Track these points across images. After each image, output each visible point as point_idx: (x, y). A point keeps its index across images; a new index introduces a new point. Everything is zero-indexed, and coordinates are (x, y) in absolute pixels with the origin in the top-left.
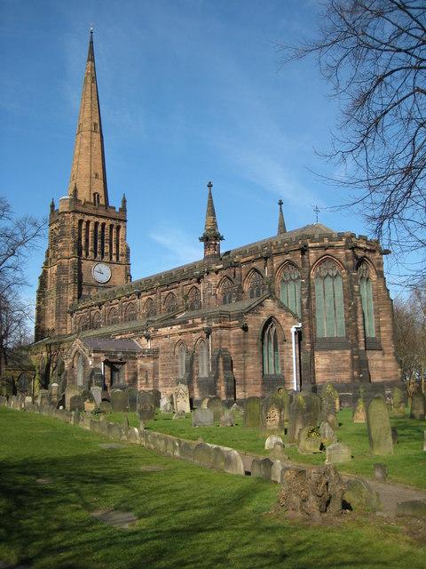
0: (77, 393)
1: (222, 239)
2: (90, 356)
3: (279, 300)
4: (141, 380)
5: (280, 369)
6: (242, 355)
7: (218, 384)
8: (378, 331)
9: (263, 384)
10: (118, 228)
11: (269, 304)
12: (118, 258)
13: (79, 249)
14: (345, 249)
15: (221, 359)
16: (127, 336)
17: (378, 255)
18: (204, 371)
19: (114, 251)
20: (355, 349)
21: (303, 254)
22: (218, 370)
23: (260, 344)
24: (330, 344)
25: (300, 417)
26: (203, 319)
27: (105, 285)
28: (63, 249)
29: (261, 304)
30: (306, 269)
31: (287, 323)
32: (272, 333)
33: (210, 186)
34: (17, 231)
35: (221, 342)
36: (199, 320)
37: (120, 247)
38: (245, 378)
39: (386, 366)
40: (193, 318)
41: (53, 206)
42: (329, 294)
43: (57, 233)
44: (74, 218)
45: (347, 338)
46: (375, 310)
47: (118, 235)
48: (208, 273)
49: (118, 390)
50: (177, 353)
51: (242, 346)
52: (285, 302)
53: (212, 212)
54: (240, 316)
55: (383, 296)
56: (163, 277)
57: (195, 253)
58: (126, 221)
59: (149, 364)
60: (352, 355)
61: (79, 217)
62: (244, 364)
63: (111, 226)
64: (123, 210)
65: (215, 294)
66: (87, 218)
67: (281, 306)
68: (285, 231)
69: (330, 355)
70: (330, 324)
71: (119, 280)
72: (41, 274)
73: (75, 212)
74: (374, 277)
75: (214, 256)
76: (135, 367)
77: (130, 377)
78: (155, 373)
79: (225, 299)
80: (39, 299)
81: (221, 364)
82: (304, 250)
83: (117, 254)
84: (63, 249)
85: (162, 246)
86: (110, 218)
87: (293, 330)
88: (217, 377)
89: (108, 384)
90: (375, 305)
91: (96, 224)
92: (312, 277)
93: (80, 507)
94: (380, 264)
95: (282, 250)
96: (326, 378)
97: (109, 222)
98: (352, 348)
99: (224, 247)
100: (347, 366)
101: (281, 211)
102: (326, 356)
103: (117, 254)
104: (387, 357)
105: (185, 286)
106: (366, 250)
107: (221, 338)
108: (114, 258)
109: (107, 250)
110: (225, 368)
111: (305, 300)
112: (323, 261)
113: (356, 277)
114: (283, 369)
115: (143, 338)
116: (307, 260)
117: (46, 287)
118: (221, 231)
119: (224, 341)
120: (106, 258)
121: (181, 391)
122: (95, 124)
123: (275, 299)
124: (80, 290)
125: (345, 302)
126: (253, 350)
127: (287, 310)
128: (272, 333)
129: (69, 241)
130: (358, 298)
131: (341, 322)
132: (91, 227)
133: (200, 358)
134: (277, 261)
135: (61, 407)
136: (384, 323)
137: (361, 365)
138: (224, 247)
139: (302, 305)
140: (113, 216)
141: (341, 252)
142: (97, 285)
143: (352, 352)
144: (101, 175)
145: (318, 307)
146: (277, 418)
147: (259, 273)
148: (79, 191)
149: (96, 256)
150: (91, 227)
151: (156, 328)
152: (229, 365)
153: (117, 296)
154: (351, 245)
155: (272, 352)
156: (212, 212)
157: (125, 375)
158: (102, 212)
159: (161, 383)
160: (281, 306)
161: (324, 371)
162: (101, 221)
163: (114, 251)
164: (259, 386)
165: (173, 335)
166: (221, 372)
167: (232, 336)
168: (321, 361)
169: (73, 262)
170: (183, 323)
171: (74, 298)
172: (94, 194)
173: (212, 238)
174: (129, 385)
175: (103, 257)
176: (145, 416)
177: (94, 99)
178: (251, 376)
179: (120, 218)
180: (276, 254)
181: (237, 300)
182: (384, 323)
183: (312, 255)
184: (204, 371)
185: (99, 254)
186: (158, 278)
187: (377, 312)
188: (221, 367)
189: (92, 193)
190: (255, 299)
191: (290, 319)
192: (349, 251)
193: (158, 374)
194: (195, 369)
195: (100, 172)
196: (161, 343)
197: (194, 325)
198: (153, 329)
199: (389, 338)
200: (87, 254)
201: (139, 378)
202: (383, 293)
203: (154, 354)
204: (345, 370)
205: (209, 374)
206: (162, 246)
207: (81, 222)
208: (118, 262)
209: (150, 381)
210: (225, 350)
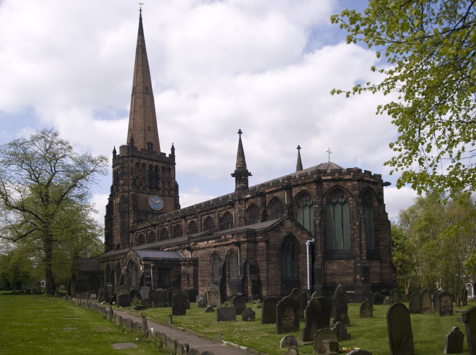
1: (250, 174)
2: (141, 263)
16: (173, 248)
31: (302, 239)
33: (240, 132)
36: (230, 236)
44: (132, 161)
61: (136, 160)
63: (163, 168)
64: (172, 156)
66: (142, 161)
68: (302, 169)
73: (133, 156)
76: (180, 271)
87: (308, 243)
88: (245, 279)
93: (292, 243)
95: (300, 182)
99: (253, 182)
100: (351, 271)
110: (252, 272)
115: (186, 250)
117: (113, 214)
118: (249, 168)
120: (161, 192)
127: (303, 229)
135: (114, 303)
138: (253, 182)
139: (315, 225)
146: (293, 318)
148: (135, 140)
151: (196, 243)
153: (167, 220)
154: (357, 178)
162: (154, 164)
164: (279, 286)
185: (154, 188)
186: (199, 206)
189: (146, 142)
191: (305, 236)
192: (356, 183)
194: (227, 273)
196: (200, 253)
197: (226, 240)
198: (193, 243)
201: (183, 280)
204: (349, 274)
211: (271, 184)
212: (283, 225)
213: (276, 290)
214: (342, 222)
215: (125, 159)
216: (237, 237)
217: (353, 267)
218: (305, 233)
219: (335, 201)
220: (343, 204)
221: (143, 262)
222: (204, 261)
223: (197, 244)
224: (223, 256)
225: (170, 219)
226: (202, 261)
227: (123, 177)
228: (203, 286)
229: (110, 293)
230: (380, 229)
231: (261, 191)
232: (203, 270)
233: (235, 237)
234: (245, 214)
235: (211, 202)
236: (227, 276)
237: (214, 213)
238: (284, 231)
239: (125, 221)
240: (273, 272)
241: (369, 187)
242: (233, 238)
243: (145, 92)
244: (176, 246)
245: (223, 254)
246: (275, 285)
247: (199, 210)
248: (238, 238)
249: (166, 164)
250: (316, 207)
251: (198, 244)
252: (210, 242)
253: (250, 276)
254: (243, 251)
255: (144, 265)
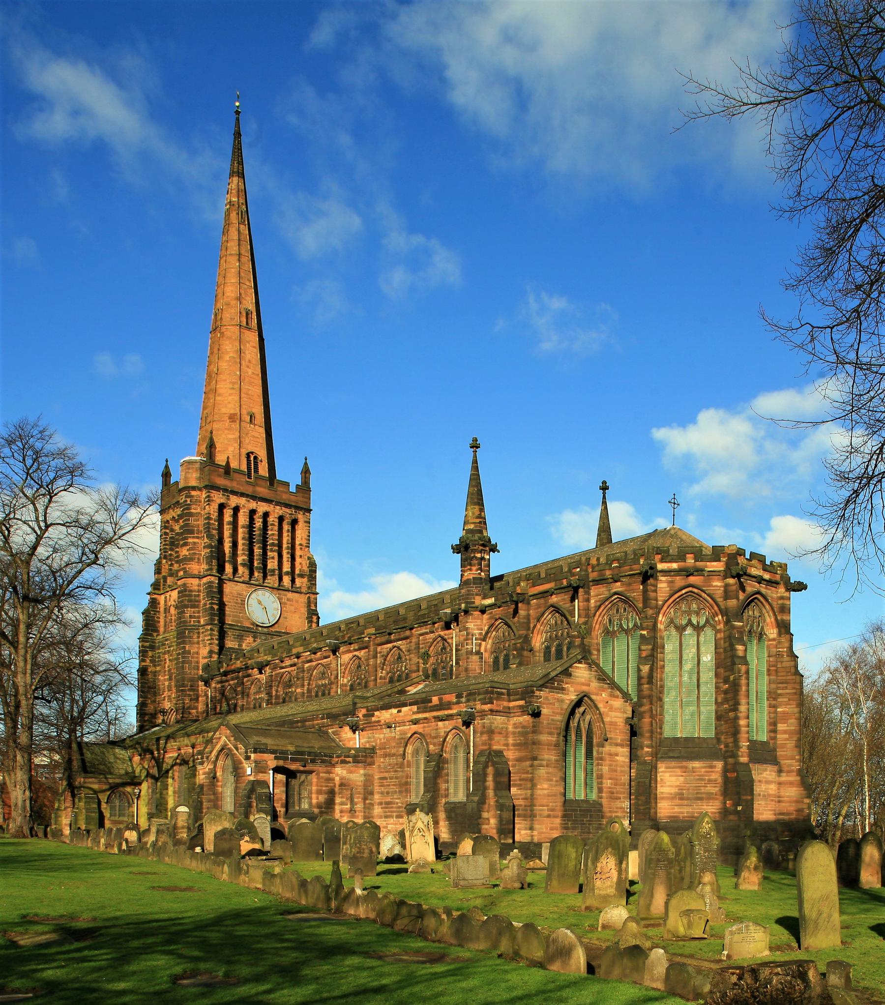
0: (227, 824)
1: (494, 549)
2: (248, 758)
3: (598, 665)
4: (342, 804)
5: (595, 791)
6: (528, 763)
7: (485, 815)
8: (773, 731)
9: (564, 816)
10: (294, 523)
11: (581, 672)
12: (293, 581)
13: (218, 558)
14: (725, 577)
15: (490, 770)
17: (782, 590)
18: (457, 789)
19: (286, 567)
20: (731, 760)
21: (644, 582)
22: (485, 788)
23: (562, 743)
24: (685, 750)
25: (662, 873)
26: (459, 696)
27: (270, 632)
28: (187, 560)
29: (566, 673)
30: (650, 612)
32: (584, 727)
33: (475, 446)
34: (101, 516)
35: (491, 739)
37: (298, 560)
38: (532, 805)
39: (782, 794)
40: (440, 693)
41: (166, 475)
42: (690, 656)
43: (177, 528)
44: (209, 500)
45: (718, 739)
46: (769, 692)
47: (293, 538)
48: (466, 612)
49: (304, 820)
50: (409, 757)
51: (528, 744)
52: (608, 669)
53: (476, 497)
54: (527, 693)
55: (787, 669)
56: (381, 617)
57: (438, 578)
58: (309, 511)
59: (357, 776)
60: (725, 771)
61: (218, 498)
62: (532, 780)
63: (281, 519)
64: (305, 488)
65: (478, 653)
66: (234, 501)
67: (604, 678)
68: (610, 540)
69: (685, 769)
70: (687, 713)
71: (297, 623)
72: (145, 604)
73: (211, 487)
74: (772, 632)
75: (477, 581)
77: (322, 798)
78: (368, 793)
79: (496, 661)
80: (143, 653)
81: (490, 778)
82: (648, 576)
83: (292, 573)
84: (187, 560)
85: (371, 568)
86: (279, 504)
88: (483, 801)
89: (281, 810)
90: (770, 682)
91: (253, 512)
92: (661, 626)
94: (785, 609)
96: (677, 809)
97: (278, 511)
98: (725, 758)
101: (604, 497)
102: (678, 772)
103: (292, 573)
104: (784, 778)
105: (424, 635)
106: (760, 580)
107: (491, 732)
108: (287, 580)
109: (272, 564)
111: (645, 669)
112: (682, 598)
113: (741, 631)
114: (600, 790)
116: (652, 595)
118: (493, 534)
119: (497, 738)
120: (272, 580)
121: (420, 825)
122: (248, 314)
123: (593, 664)
124: (222, 636)
125: (717, 675)
126: (549, 756)
127: (614, 685)
128: (584, 727)
129: (201, 544)
130: (743, 668)
131: (708, 710)
132: (243, 520)
133: (451, 766)
134: (597, 593)
136: (785, 717)
137: (737, 787)
138: (499, 565)
139: (640, 678)
140: (285, 497)
141: (717, 583)
142: (254, 630)
143: (726, 764)
144: (260, 418)
145: (668, 684)
147: (563, 615)
148: (219, 446)
149: (251, 574)
150: (243, 520)
152: (504, 783)
153: (295, 651)
155: (583, 759)
156: (476, 497)
157: (311, 797)
158: (263, 491)
159: (377, 810)
160: (604, 678)
161: (672, 797)
162: (262, 508)
163: (286, 567)
164: (558, 821)
165: (403, 723)
166: (491, 793)
167: (511, 728)
168: (669, 780)
169: (210, 585)
170: (422, 702)
171: (211, 652)
172: (248, 456)
173: (473, 547)
174: (321, 813)
175: (265, 577)
176: (360, 865)
177: (246, 259)
178: (545, 802)
179: (300, 504)
180: (597, 582)
181: (520, 664)
182: (785, 717)
183: (663, 585)
184: (457, 789)
185: (258, 572)
187: (773, 696)
188: (490, 782)
189: (244, 452)
190: (554, 663)
192: (731, 581)
193: (372, 793)
194: (443, 786)
195: (259, 411)
196: (381, 736)
197: (441, 706)
198: (364, 711)
199: (791, 744)
200: (235, 570)
201: (338, 800)
202: (786, 662)
203: (364, 757)
204: (710, 797)
205: (468, 795)
206: (371, 568)
207: (222, 507)
208: (294, 589)
209: (359, 806)
210: (499, 753)
211: (543, 575)
212: (570, 675)
213: (552, 829)
214: (698, 673)
215: (193, 493)
216: (468, 701)
217: (720, 780)
218: (617, 697)
219: (684, 622)
220: (698, 629)
221: (253, 756)
222: (391, 755)
223: (373, 715)
224: (434, 745)
225: (301, 649)
226: (385, 756)
227: (186, 538)
228: (386, 817)
229: (183, 827)
230: (779, 692)
231: (519, 590)
232: (385, 778)
233: (463, 700)
234: (480, 645)
235: (402, 611)
236: (442, 792)
237: (406, 638)
238: (572, 689)
239: (189, 652)
240: (545, 786)
241: (758, 593)
242: (458, 703)
243: (244, 324)
244: (323, 718)
245: (436, 741)
246: (549, 816)
247: (373, 631)
248: (471, 704)
249: (288, 511)
250: (642, 636)
251: (376, 713)
252: (404, 709)
253: (496, 795)
254: (482, 733)
255: (256, 762)
